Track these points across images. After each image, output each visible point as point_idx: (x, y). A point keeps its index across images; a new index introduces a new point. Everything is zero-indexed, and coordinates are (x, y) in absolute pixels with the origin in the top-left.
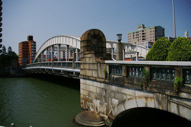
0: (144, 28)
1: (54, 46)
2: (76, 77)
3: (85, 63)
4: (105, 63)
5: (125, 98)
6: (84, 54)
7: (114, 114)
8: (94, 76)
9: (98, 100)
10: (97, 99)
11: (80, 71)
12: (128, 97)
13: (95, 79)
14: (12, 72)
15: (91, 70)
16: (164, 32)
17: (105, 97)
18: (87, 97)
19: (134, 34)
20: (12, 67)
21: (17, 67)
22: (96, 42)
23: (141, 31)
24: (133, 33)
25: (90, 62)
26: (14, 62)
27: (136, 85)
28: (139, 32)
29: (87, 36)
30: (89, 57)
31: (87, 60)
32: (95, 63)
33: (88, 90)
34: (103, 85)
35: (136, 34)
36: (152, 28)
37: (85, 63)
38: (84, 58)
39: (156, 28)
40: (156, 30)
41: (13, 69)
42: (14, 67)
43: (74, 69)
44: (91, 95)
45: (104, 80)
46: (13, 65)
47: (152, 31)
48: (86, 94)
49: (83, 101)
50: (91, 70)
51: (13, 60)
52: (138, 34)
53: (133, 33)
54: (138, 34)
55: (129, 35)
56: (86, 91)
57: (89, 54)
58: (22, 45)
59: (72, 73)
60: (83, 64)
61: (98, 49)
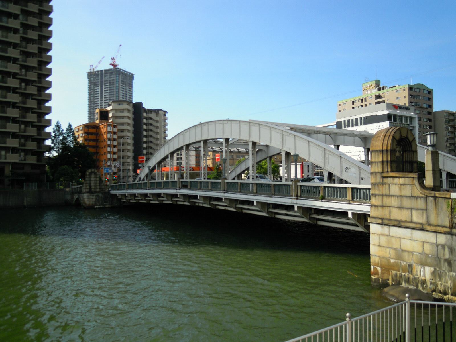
0: (379, 90)
2: (258, 211)
3: (386, 195)
4: (450, 198)
6: (383, 177)
11: (369, 210)
14: (87, 199)
15: (408, 209)
16: (430, 99)
20: (88, 187)
21: (98, 187)
24: (353, 102)
26: (93, 176)
29: (390, 141)
30: (400, 184)
32: (420, 197)
33: (395, 246)
37: (386, 195)
39: (411, 88)
40: (412, 93)
41: (90, 192)
42: (93, 187)
43: (297, 199)
44: (407, 258)
45: (447, 230)
46: (90, 183)
48: (388, 255)
50: (408, 209)
51: (92, 172)
52: (364, 104)
53: (353, 102)
54: (364, 104)
55: (342, 107)
56: (388, 249)
57: (399, 177)
58: (85, 133)
61: (403, 165)
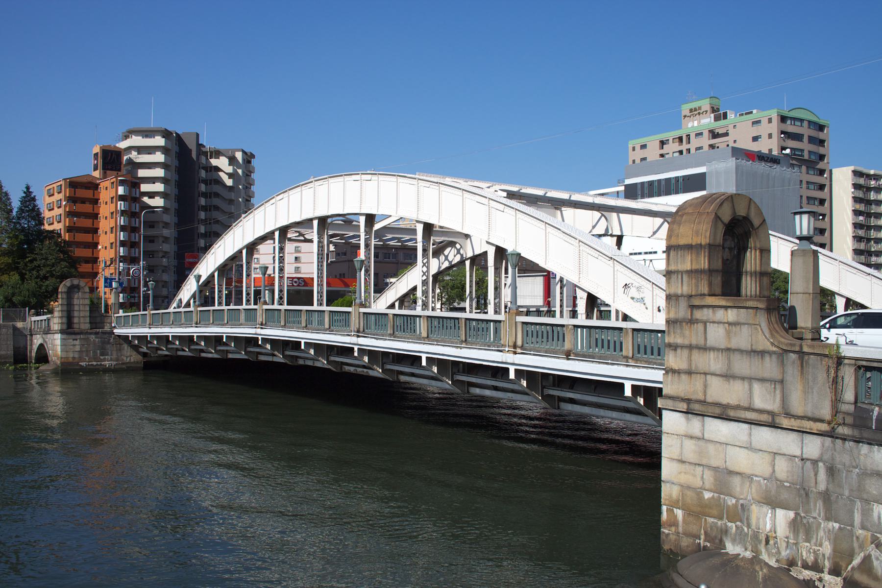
0: (717, 119)
1: (329, 220)
8: (758, 403)
9: (780, 513)
10: (773, 502)
13: (824, 427)
15: (743, 379)
17: (826, 497)
18: (707, 495)
19: (667, 148)
22: (730, 249)
23: (706, 134)
24: (663, 143)
25: (733, 344)
28: (692, 136)
30: (730, 324)
31: (716, 335)
32: (770, 353)
33: (714, 463)
34: (813, 447)
35: (676, 147)
36: (764, 121)
38: (692, 321)
47: (765, 136)
49: (679, 513)
52: (684, 147)
53: (663, 143)
54: (684, 147)
57: (726, 308)
59: (347, 351)
60: (686, 352)
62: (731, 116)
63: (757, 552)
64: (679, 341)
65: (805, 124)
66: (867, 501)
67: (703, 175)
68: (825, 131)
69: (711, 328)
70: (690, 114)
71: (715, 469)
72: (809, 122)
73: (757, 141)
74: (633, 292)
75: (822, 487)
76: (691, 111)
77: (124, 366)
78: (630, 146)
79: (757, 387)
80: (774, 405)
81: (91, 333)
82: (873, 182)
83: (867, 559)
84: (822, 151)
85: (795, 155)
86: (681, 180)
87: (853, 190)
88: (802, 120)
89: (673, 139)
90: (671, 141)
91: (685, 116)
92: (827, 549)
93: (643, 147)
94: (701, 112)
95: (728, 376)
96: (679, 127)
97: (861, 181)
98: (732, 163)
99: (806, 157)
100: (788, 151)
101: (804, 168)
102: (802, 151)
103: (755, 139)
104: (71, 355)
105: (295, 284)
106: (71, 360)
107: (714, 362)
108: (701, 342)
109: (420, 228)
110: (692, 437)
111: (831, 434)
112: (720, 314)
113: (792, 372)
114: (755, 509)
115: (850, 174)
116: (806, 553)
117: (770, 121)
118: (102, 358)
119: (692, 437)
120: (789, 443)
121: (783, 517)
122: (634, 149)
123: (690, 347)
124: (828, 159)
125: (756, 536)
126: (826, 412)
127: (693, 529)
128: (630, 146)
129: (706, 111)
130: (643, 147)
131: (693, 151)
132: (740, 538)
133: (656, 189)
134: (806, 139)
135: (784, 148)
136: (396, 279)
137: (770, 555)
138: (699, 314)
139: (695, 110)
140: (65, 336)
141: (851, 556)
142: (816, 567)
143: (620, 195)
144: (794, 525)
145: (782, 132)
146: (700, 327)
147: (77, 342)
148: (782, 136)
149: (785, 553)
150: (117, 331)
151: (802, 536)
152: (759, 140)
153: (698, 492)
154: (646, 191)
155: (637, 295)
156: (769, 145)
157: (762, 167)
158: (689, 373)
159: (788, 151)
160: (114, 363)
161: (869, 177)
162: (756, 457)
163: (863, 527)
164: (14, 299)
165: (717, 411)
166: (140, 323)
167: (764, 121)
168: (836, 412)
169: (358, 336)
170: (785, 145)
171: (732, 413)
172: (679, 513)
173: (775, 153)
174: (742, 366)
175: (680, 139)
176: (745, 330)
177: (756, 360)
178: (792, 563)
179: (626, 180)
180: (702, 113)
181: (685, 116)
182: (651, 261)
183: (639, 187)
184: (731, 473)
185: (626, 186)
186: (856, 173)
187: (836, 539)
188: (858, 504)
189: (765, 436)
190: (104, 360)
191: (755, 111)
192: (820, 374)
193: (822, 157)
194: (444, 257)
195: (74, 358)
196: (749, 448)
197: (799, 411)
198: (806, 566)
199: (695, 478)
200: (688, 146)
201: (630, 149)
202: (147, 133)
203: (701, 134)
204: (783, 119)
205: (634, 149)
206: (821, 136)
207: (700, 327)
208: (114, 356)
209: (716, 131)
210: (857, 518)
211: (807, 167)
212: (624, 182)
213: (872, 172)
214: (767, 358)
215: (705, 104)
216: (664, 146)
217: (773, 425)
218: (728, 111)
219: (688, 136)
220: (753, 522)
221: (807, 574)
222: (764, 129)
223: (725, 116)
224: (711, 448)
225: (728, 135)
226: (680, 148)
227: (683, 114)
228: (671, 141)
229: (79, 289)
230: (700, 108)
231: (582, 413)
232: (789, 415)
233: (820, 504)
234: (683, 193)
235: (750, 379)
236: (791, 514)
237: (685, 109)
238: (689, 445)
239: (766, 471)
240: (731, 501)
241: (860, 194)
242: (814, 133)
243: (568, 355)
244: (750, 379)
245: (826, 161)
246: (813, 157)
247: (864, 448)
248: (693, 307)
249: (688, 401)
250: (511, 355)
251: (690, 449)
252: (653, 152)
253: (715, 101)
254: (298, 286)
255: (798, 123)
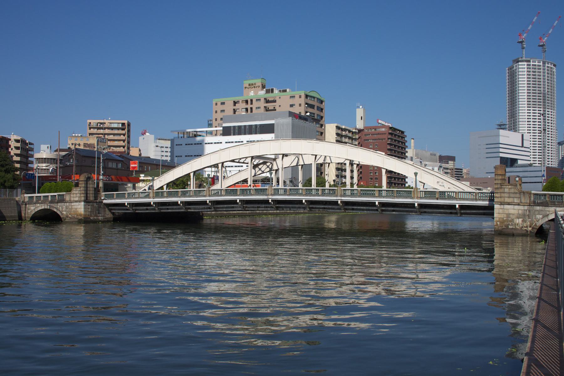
3: (503, 193)
5: (548, 213)
7: (538, 225)
8: (515, 201)
9: (520, 219)
12: (551, 212)
13: (528, 204)
15: (512, 197)
23: (263, 100)
24: (235, 103)
25: (510, 192)
27: (557, 205)
31: (506, 190)
33: (506, 213)
34: (526, 208)
35: (244, 105)
36: (297, 97)
38: (501, 188)
47: (297, 105)
49: (499, 223)
52: (249, 106)
53: (235, 103)
54: (249, 106)
60: (500, 193)
62: (276, 91)
63: (515, 227)
64: (498, 192)
65: (316, 99)
66: (535, 215)
67: (273, 125)
68: (323, 104)
69: (505, 189)
70: (249, 87)
71: (507, 214)
72: (317, 99)
73: (293, 107)
74: (440, 184)
75: (528, 214)
76: (249, 85)
77: (106, 220)
78: (214, 102)
79: (515, 199)
80: (519, 202)
81: (94, 202)
82: (344, 133)
83: (536, 224)
84: (322, 114)
85: (311, 116)
86: (258, 127)
87: (336, 136)
88: (314, 98)
89: (242, 101)
90: (241, 102)
91: (246, 88)
92: (529, 223)
93: (223, 103)
94: (256, 86)
95: (509, 197)
96: (242, 95)
97: (339, 132)
98: (289, 120)
99: (316, 118)
100: (308, 114)
101: (314, 123)
102: (314, 114)
103: (292, 106)
104: (87, 213)
105: (107, 180)
106: (87, 216)
107: (506, 195)
108: (503, 191)
109: (348, 163)
110: (501, 209)
111: (530, 205)
112: (507, 187)
113: (522, 196)
114: (515, 219)
115: (335, 127)
116: (525, 225)
117: (300, 97)
118: (98, 215)
119: (501, 209)
120: (521, 207)
121: (520, 220)
122: (216, 104)
123: (501, 193)
124: (324, 119)
125: (515, 224)
126: (528, 202)
127: (502, 225)
128: (214, 102)
129: (259, 86)
130: (223, 103)
131: (254, 109)
132: (512, 225)
133: (243, 131)
134: (316, 108)
135: (306, 112)
136: (157, 178)
137: (518, 227)
138: (502, 187)
139: (252, 85)
140: (85, 204)
141: (533, 224)
142: (527, 227)
143: (219, 133)
144: (523, 221)
145: (306, 104)
146: (503, 189)
147: (90, 207)
148: (306, 105)
149: (521, 226)
150: (105, 201)
151: (524, 222)
152: (294, 106)
153: (503, 218)
154: (237, 131)
155: (441, 184)
156: (300, 110)
157: (301, 122)
158: (501, 197)
159: (308, 114)
160: (102, 218)
161: (342, 130)
162: (515, 211)
163: (535, 219)
164: (6, 184)
165: (507, 203)
166: (160, 196)
167: (297, 97)
168: (530, 201)
169: (341, 197)
170: (307, 110)
171: (510, 204)
172: (499, 223)
173: (303, 114)
174: (512, 195)
175: (247, 102)
176: (513, 189)
177: (515, 194)
178: (522, 227)
179: (223, 124)
180: (257, 87)
181: (246, 88)
182: (230, 171)
183: (232, 128)
184: (510, 214)
185: (224, 127)
186: (338, 128)
187: (530, 222)
188: (534, 216)
189: (516, 207)
190: (99, 216)
191: (288, 90)
192: (527, 196)
193: (322, 117)
194: (258, 169)
195: (88, 215)
196: (514, 209)
197: (523, 202)
198: (525, 227)
199: (502, 216)
200: (251, 106)
201: (214, 104)
202: (535, 166)
203: (259, 100)
204: (307, 96)
205: (216, 104)
206: (322, 106)
207: (503, 189)
208: (103, 215)
209: (268, 99)
210: (534, 218)
211: (316, 123)
212: (222, 125)
213: (343, 127)
214: (517, 194)
215: (258, 82)
216: (236, 104)
217: (519, 205)
218: (274, 88)
219: (252, 100)
220: (515, 221)
221: (525, 228)
222: (297, 101)
223: (272, 91)
224: (506, 210)
225: (276, 102)
226: (246, 106)
227: (245, 86)
228: (241, 102)
229: (90, 179)
230: (255, 84)
231: (421, 217)
232: (522, 203)
233: (527, 217)
234: (249, 134)
235: (514, 198)
236: (522, 219)
237: (246, 83)
238: (501, 210)
239: (517, 213)
240: (510, 219)
241: (339, 139)
242: (319, 105)
243: (437, 199)
244: (514, 198)
245: (323, 120)
246: (318, 118)
247: (535, 207)
248: (501, 185)
249: (501, 202)
250: (417, 200)
251: (501, 211)
252: (229, 108)
253: (264, 81)
254: (109, 180)
255: (313, 99)
